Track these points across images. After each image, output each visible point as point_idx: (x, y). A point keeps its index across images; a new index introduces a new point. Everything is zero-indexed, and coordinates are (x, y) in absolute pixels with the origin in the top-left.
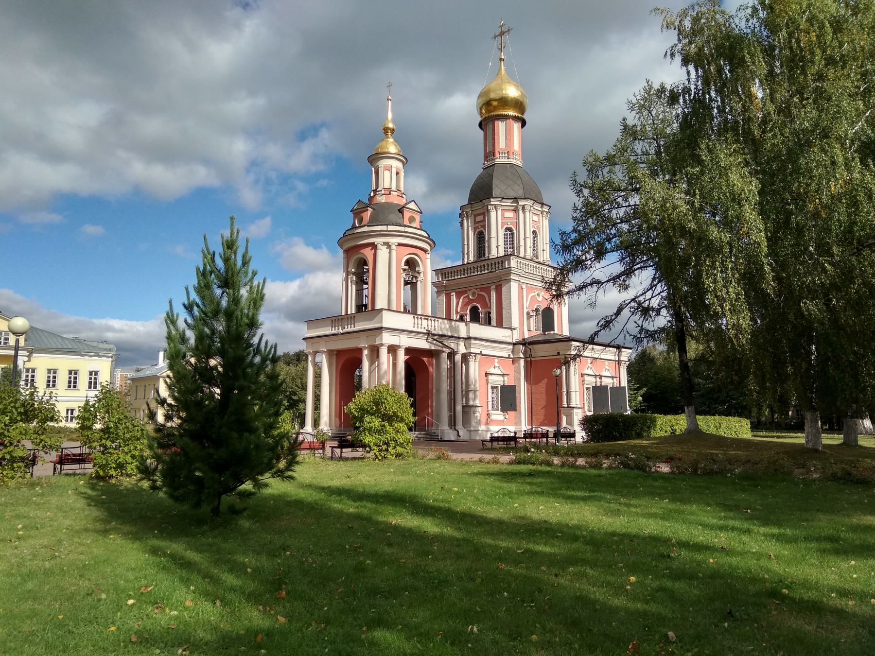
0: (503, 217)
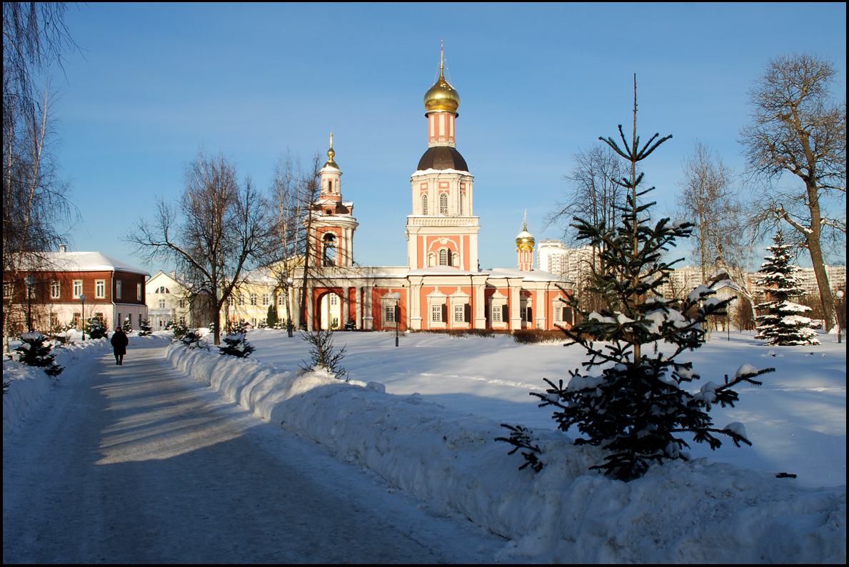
0: (440, 187)
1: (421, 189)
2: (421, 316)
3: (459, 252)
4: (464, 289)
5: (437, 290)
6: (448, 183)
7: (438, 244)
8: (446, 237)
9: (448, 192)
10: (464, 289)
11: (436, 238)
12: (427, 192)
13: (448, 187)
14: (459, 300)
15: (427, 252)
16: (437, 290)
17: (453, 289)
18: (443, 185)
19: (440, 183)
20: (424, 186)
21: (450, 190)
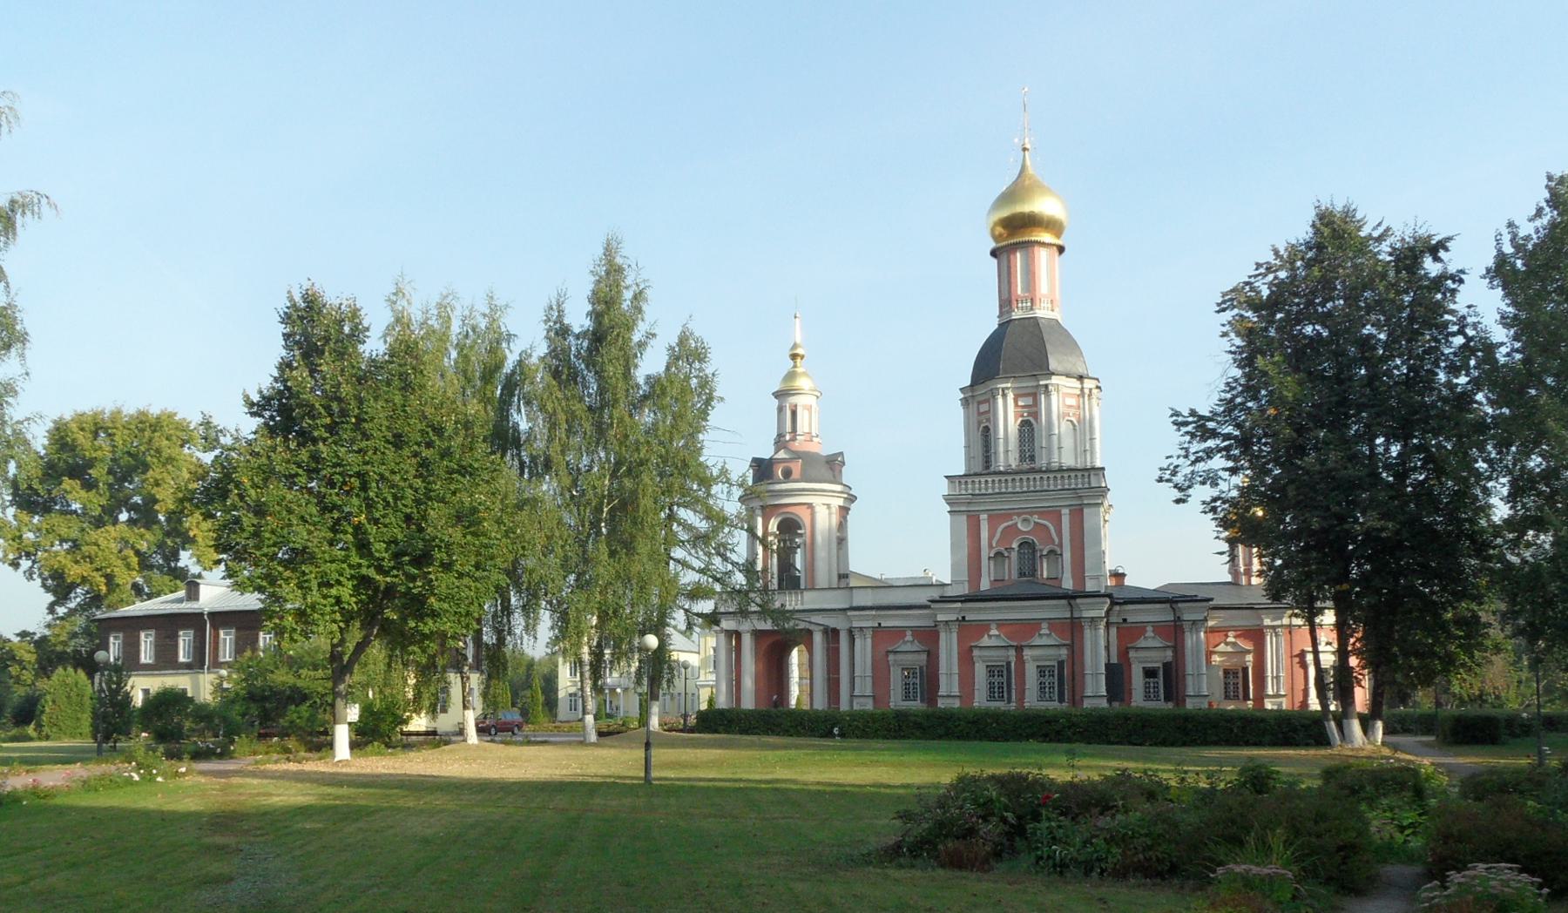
1: (980, 414)
3: (1061, 545)
4: (1159, 629)
5: (1150, 633)
7: (1012, 531)
8: (1031, 514)
10: (1159, 629)
11: (1008, 516)
12: (988, 420)
14: (1044, 649)
15: (990, 546)
16: (1150, 633)
17: (1032, 626)
18: (184, 641)
20: (984, 408)
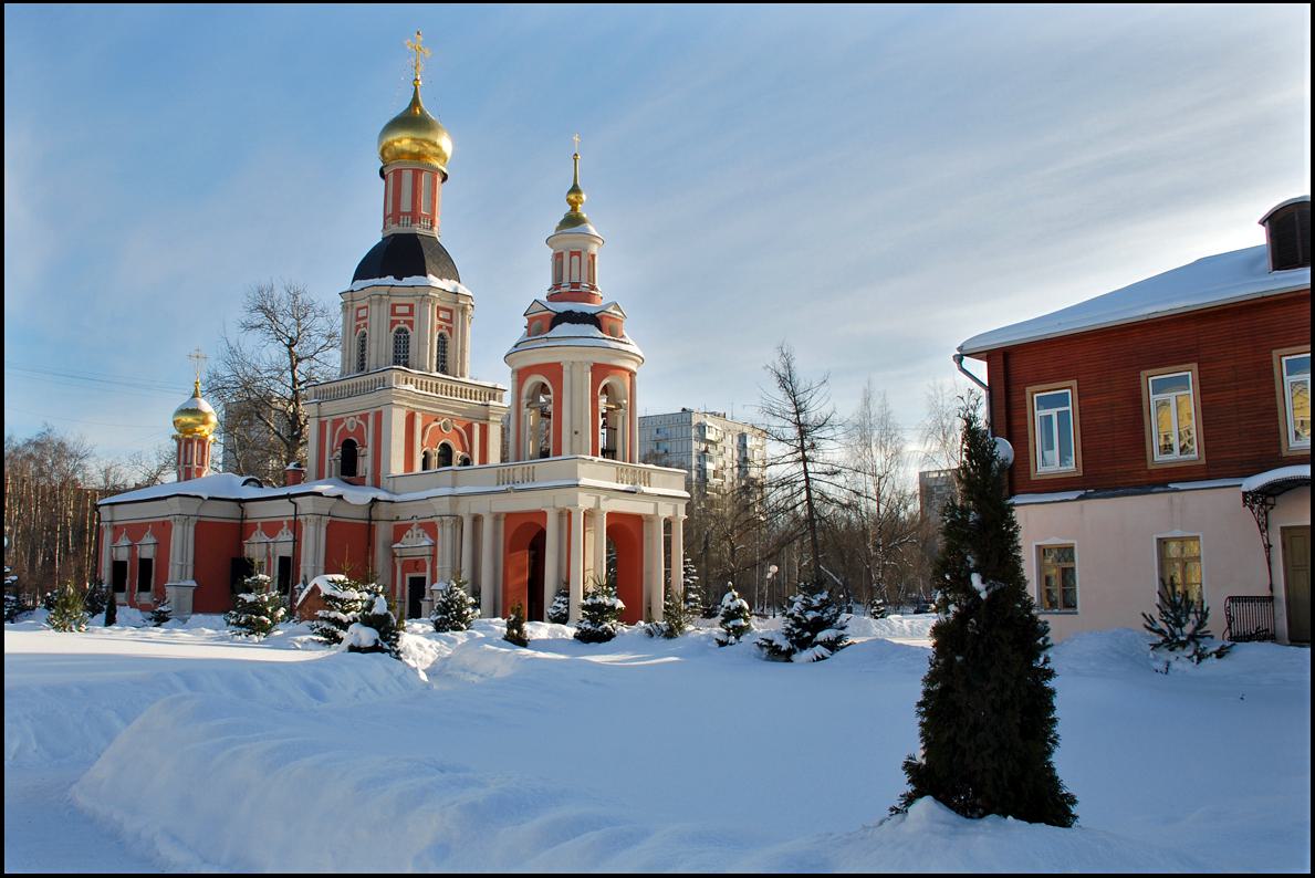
0: (393, 313)
2: (194, 578)
6: (411, 306)
9: (411, 324)
12: (365, 325)
13: (411, 313)
18: (399, 310)
19: (394, 306)
21: (415, 319)
